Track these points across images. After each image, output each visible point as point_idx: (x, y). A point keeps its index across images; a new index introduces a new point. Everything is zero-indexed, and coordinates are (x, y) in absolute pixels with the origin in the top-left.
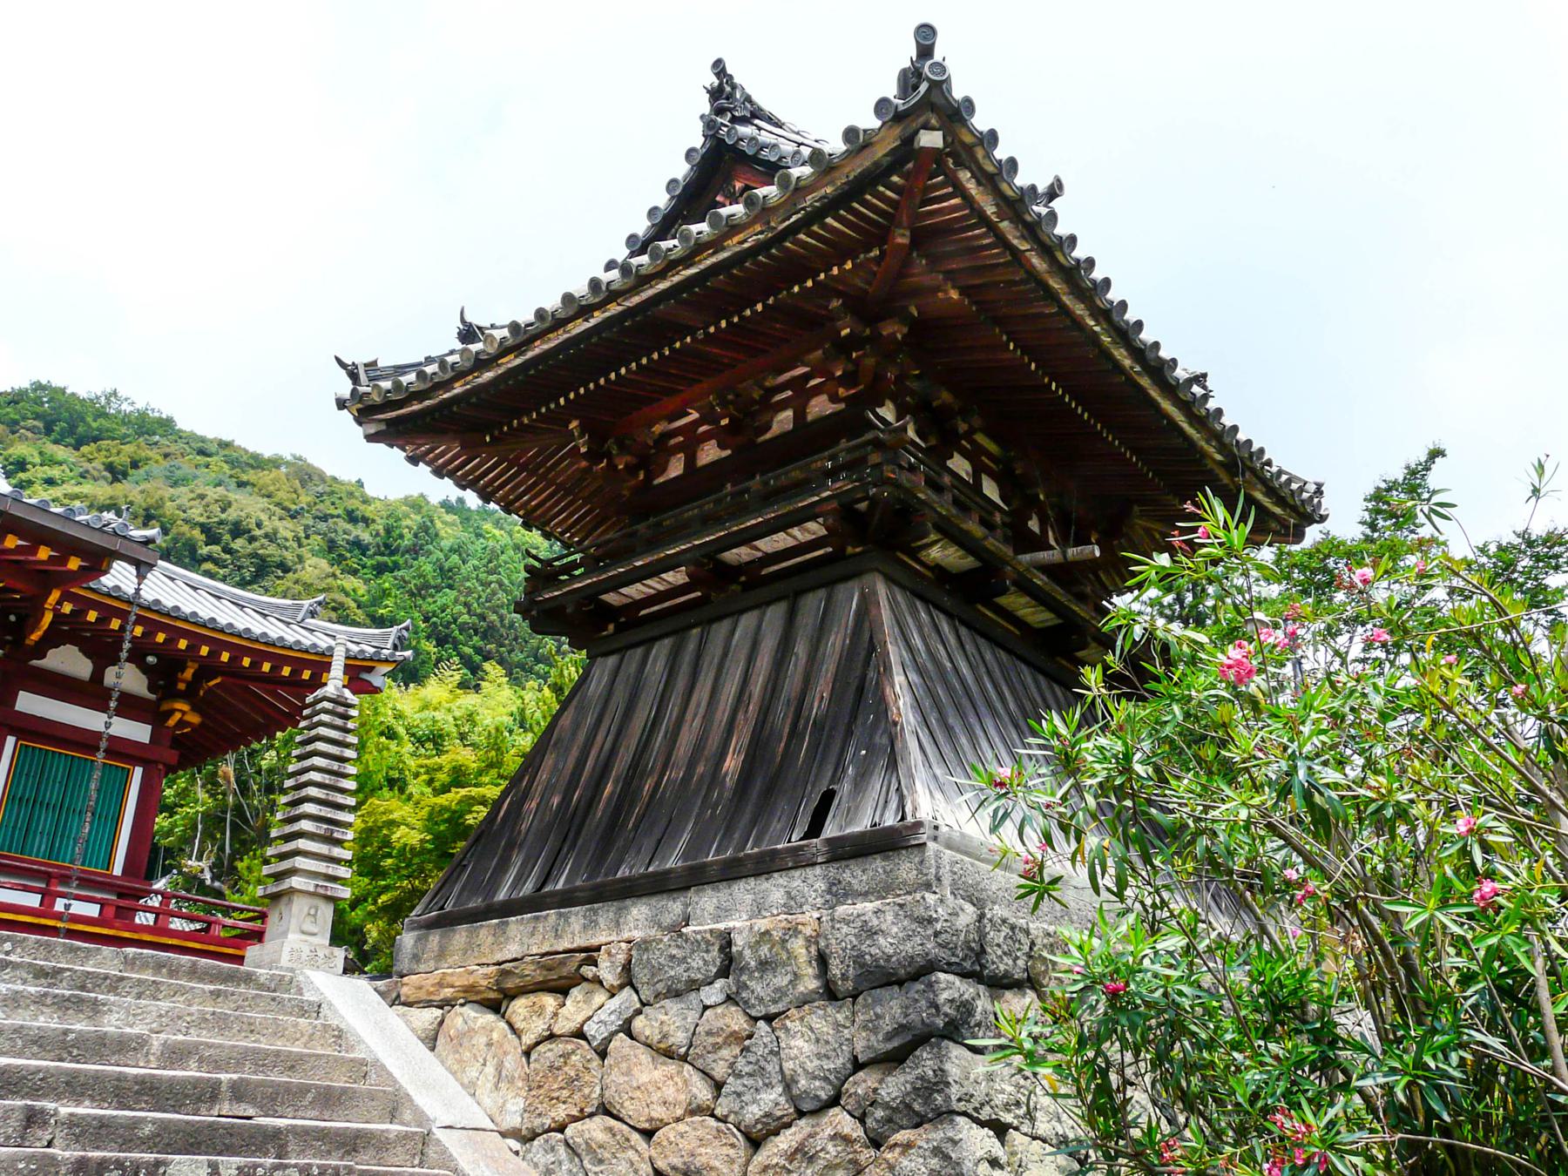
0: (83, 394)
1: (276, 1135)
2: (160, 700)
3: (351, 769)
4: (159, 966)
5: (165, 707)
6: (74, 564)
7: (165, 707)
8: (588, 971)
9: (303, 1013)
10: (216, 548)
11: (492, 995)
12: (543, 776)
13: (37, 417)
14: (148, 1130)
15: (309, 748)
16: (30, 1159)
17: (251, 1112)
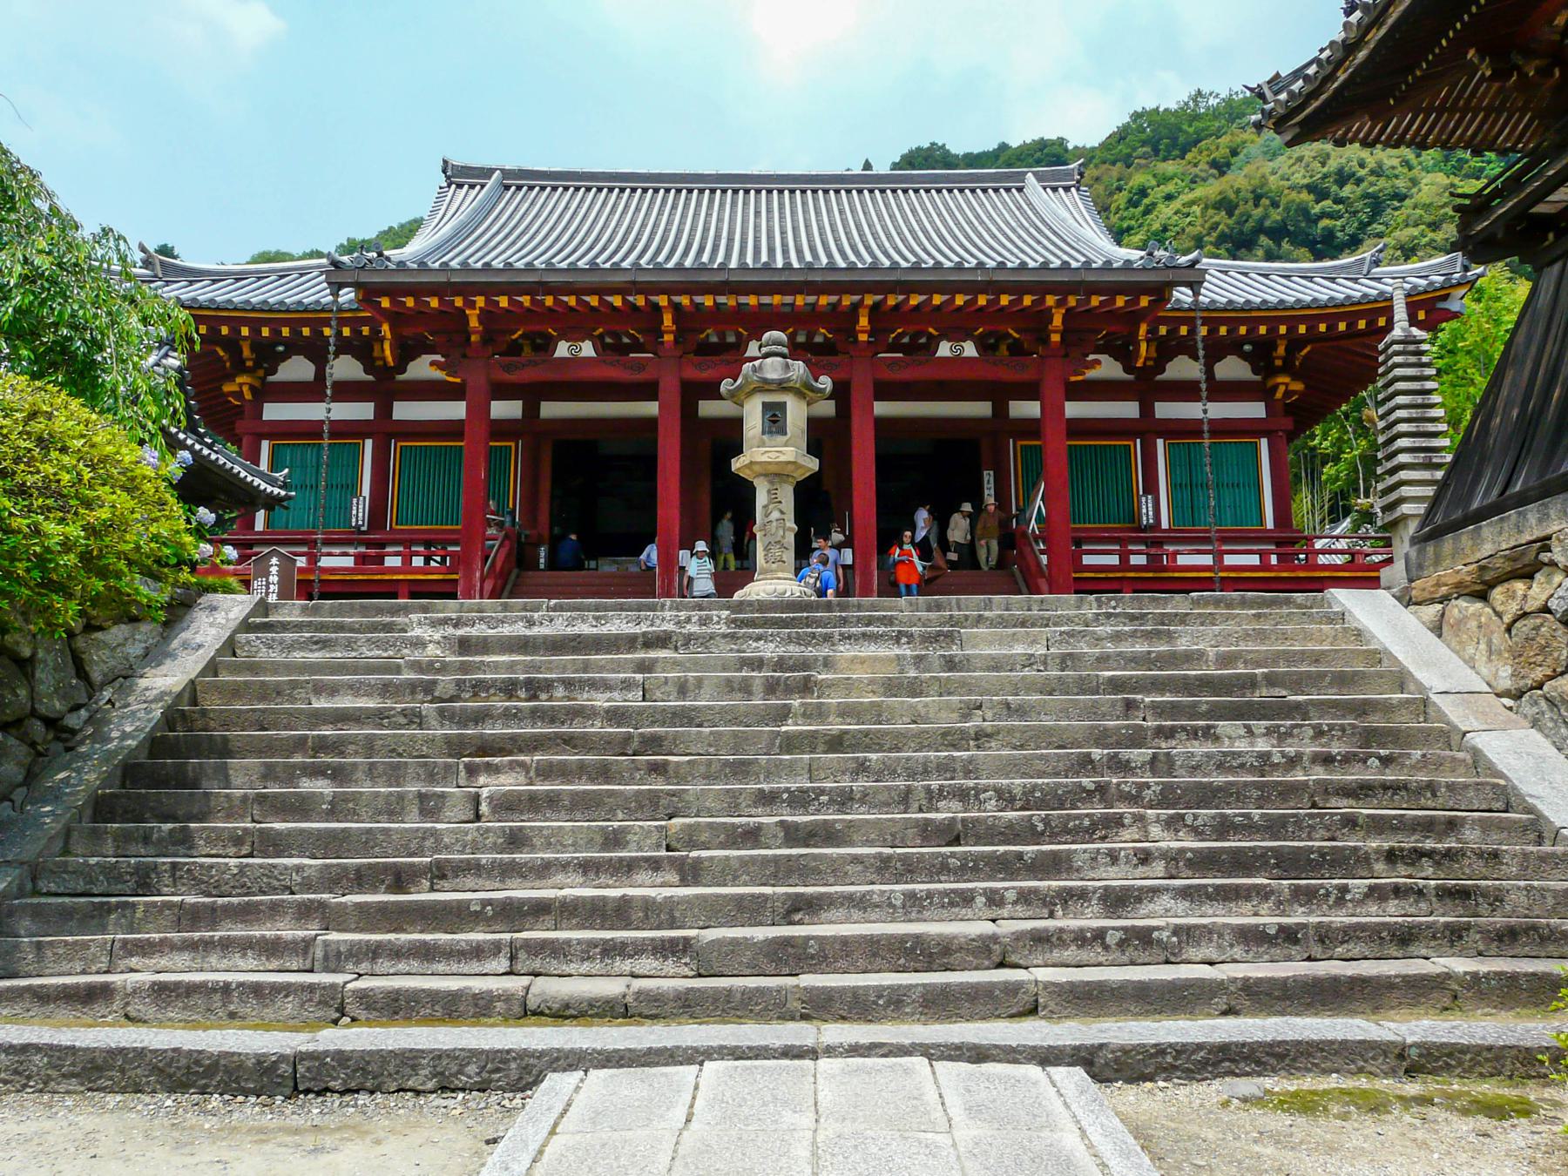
0: (1173, 106)
1: (1298, 706)
2: (1265, 379)
3: (1436, 398)
4: (1217, 603)
5: (1270, 383)
6: (1144, 302)
7: (1270, 383)
8: (1545, 557)
9: (1331, 621)
10: (1328, 203)
11: (1478, 588)
12: (1504, 392)
13: (1144, 143)
14: (1204, 708)
15: (1391, 390)
16: (1127, 727)
17: (1284, 693)
